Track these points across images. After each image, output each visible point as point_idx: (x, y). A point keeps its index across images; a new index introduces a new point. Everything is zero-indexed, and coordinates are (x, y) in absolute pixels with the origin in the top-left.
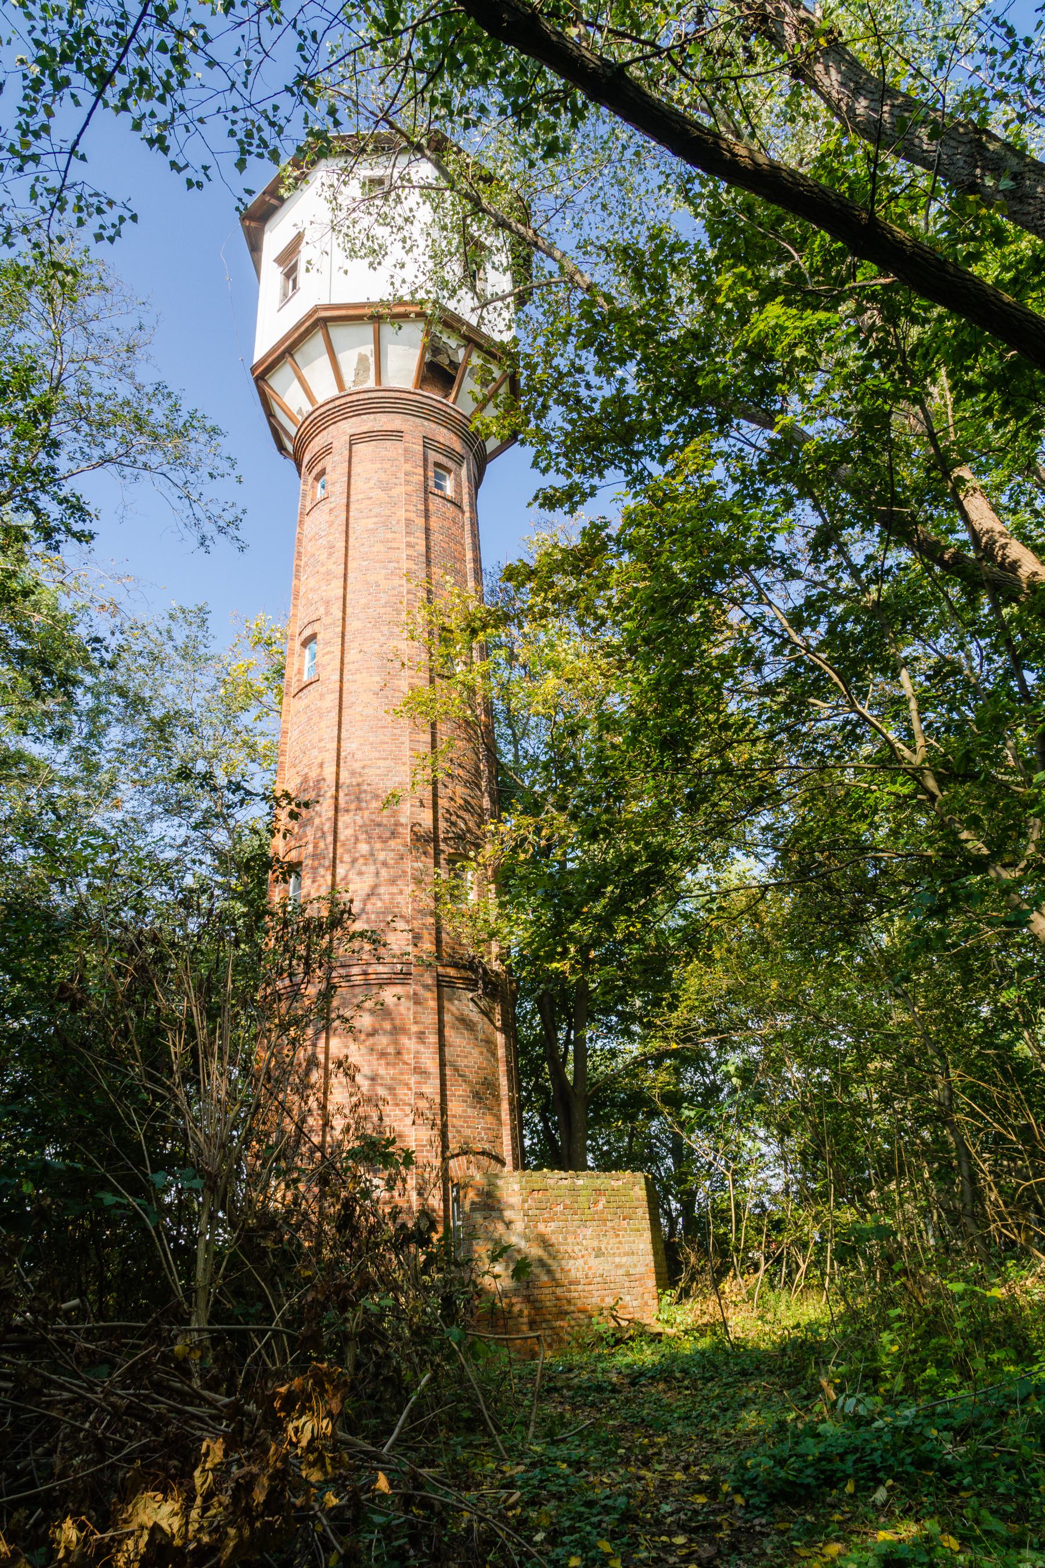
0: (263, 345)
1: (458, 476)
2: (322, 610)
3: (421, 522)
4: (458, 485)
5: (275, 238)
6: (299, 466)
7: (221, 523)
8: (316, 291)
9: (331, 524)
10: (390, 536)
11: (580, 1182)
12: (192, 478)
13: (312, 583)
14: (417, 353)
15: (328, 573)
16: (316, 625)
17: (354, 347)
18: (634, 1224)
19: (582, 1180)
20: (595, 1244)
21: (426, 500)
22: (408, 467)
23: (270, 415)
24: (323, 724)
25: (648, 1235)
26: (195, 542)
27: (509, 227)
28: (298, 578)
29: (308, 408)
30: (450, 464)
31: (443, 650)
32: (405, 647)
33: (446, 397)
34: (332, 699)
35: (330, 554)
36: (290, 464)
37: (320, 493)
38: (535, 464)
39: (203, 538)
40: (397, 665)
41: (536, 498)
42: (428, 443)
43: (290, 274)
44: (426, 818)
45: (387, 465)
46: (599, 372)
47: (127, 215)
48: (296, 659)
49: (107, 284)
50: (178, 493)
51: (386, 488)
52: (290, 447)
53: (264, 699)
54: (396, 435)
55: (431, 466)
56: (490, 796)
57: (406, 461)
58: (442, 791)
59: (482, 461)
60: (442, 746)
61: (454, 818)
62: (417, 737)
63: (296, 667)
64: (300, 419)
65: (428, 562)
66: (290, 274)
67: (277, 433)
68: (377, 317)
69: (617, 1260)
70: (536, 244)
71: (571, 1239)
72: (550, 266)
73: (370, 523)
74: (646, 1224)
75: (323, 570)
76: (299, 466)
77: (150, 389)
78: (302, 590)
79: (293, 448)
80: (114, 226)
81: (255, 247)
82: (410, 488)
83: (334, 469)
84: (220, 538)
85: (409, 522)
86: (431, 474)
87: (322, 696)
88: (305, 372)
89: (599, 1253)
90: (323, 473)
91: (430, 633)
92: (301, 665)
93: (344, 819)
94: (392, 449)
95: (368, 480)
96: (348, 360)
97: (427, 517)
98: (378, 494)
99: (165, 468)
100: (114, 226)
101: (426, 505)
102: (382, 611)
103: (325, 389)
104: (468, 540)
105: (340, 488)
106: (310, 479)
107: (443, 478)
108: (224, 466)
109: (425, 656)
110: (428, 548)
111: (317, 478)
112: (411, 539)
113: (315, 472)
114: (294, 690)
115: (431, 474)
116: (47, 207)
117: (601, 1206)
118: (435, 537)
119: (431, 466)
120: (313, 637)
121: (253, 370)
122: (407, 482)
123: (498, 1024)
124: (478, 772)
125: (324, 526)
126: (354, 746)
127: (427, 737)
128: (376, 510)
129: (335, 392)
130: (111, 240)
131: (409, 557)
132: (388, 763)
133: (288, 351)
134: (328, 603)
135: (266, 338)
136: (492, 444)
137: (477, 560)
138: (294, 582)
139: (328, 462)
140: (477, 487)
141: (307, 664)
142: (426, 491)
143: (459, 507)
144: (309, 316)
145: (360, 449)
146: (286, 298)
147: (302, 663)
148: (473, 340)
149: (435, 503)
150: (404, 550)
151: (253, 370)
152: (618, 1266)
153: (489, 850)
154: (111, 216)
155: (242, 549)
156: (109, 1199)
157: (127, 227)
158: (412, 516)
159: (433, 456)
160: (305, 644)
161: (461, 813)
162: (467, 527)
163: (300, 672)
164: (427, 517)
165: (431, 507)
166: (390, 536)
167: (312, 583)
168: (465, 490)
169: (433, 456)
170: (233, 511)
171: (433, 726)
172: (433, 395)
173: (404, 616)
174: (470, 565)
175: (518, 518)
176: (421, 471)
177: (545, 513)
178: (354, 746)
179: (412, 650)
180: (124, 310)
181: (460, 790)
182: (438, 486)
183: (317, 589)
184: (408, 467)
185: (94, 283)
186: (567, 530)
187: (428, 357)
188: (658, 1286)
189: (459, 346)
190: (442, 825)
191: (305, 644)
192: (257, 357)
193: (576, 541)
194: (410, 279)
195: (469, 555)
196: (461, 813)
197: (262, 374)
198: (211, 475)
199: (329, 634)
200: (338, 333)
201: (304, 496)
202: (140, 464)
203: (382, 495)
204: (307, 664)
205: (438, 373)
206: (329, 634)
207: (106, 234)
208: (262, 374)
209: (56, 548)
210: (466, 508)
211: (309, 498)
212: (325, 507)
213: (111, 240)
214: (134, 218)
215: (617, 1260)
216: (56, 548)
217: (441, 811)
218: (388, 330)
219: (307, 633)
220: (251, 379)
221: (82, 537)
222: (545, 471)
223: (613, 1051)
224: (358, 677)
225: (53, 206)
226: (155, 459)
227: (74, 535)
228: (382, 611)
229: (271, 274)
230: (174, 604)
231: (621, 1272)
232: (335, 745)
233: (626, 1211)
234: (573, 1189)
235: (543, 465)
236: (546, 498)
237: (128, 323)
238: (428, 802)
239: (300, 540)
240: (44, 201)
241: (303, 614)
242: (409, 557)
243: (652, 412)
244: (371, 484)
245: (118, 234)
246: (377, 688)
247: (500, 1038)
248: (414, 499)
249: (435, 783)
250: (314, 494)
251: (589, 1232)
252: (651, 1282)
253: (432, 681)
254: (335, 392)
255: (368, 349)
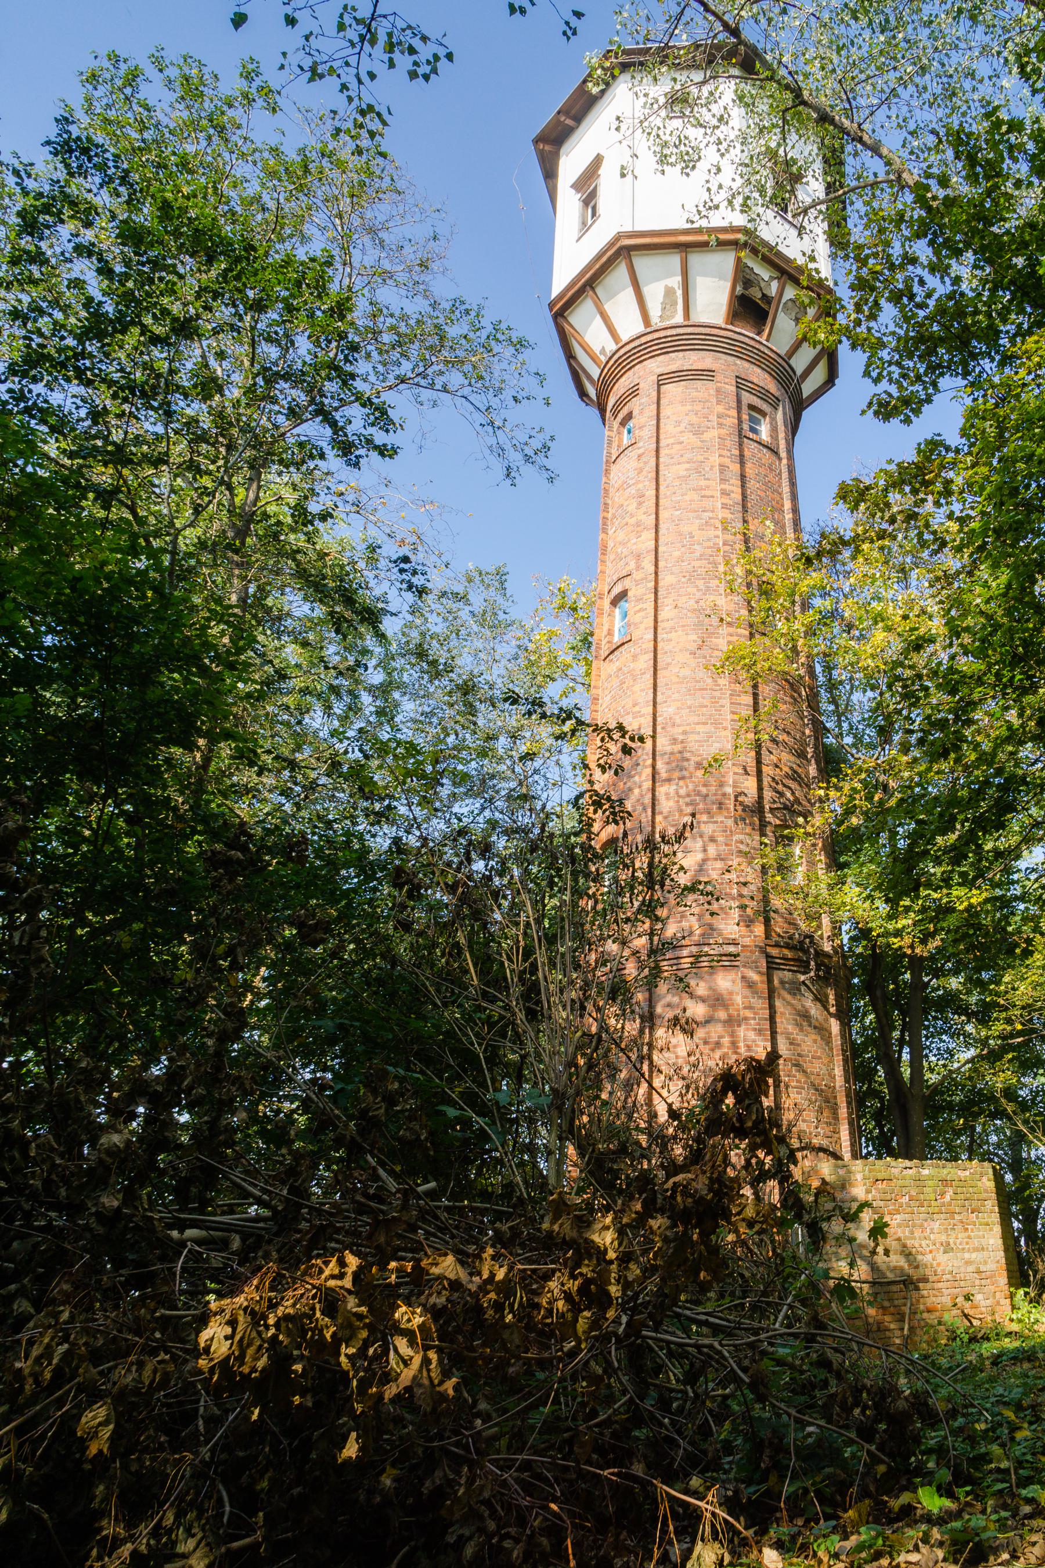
0: (561, 279)
1: (773, 420)
2: (632, 565)
3: (736, 468)
4: (774, 429)
5: (571, 163)
6: (602, 411)
7: (529, 451)
8: (622, 212)
9: (640, 471)
10: (703, 483)
11: (926, 1172)
12: (495, 402)
13: (621, 536)
14: (728, 285)
15: (638, 524)
16: (627, 581)
17: (660, 278)
18: (984, 1217)
19: (929, 1170)
20: (944, 1238)
21: (741, 445)
22: (720, 409)
23: (570, 356)
24: (637, 688)
25: (997, 1229)
26: (502, 472)
27: (832, 121)
28: (605, 531)
29: (611, 346)
30: (765, 407)
31: (764, 604)
32: (723, 602)
33: (759, 334)
34: (645, 661)
35: (640, 504)
36: (595, 412)
37: (626, 440)
38: (867, 374)
39: (508, 468)
40: (715, 620)
41: (870, 404)
42: (741, 383)
43: (590, 200)
44: (750, 785)
45: (698, 407)
46: (933, 269)
47: (442, 52)
48: (605, 619)
49: (401, 185)
50: (480, 418)
51: (698, 432)
52: (592, 392)
53: (570, 672)
54: (707, 374)
55: (745, 408)
56: (818, 763)
57: (719, 402)
58: (766, 758)
59: (799, 405)
60: (765, 706)
61: (780, 787)
62: (738, 700)
63: (605, 628)
64: (603, 359)
65: (745, 509)
66: (590, 200)
67: (577, 375)
68: (683, 246)
69: (967, 1255)
70: (860, 140)
71: (917, 1233)
72: (875, 166)
73: (681, 470)
74: (995, 1218)
75: (633, 521)
76: (602, 411)
77: (447, 306)
78: (610, 544)
79: (597, 394)
80: (428, 62)
81: (550, 174)
82: (723, 431)
83: (641, 412)
84: (527, 470)
85: (723, 468)
86: (745, 417)
87: (635, 657)
88: (607, 307)
89: (947, 1248)
90: (629, 416)
91: (749, 585)
92: (611, 625)
93: (662, 790)
94: (702, 389)
95: (678, 423)
96: (654, 293)
97: (742, 463)
98: (689, 438)
99: (466, 391)
100: (428, 62)
101: (741, 450)
102: (697, 564)
103: (630, 326)
104: (786, 489)
105: (649, 432)
106: (616, 424)
107: (758, 423)
108: (530, 384)
109: (744, 612)
110: (744, 496)
111: (623, 424)
112: (726, 487)
113: (621, 416)
114: (604, 653)
115: (745, 417)
116: (356, 40)
117: (948, 1198)
118: (752, 485)
119: (745, 408)
120: (623, 595)
121: (551, 306)
122: (720, 425)
123: (833, 1010)
124: (804, 744)
125: (631, 474)
126: (671, 710)
127: (749, 700)
128: (688, 456)
129: (640, 328)
130: (426, 77)
131: (724, 506)
132: (709, 728)
133: (588, 284)
134: (638, 557)
135: (564, 274)
136: (808, 388)
137: (795, 510)
138: (602, 536)
139: (635, 405)
140: (794, 434)
141: (618, 624)
142: (741, 435)
143: (776, 453)
144: (611, 244)
145: (671, 390)
146: (585, 227)
147: (612, 623)
148: (787, 271)
149: (750, 448)
150: (719, 498)
151: (551, 306)
152: (968, 1263)
153: (818, 820)
154: (425, 52)
155: (551, 480)
156: (452, 1112)
157: (443, 65)
158: (727, 461)
159: (747, 398)
160: (614, 603)
161: (786, 781)
162: (785, 475)
163: (610, 633)
164: (742, 463)
165: (746, 453)
166: (703, 483)
167: (621, 536)
168: (782, 435)
169: (747, 398)
170: (541, 436)
171: (755, 686)
172: (746, 332)
173: (722, 568)
174: (788, 516)
175: (849, 439)
176: (734, 413)
177: (877, 424)
178: (671, 710)
179: (729, 604)
180: (417, 218)
181: (785, 756)
182: (753, 430)
183: (627, 541)
184: (720, 409)
185: (386, 183)
186: (901, 443)
187: (739, 289)
188: (1010, 1284)
189: (772, 278)
190: (768, 794)
191: (614, 603)
192: (555, 292)
193: (910, 456)
194: (727, 182)
195: (787, 505)
196: (786, 781)
197: (561, 311)
198: (515, 399)
199: (640, 590)
200: (643, 264)
201: (610, 442)
202: (438, 387)
203: (693, 439)
204: (618, 624)
205: (750, 308)
206: (640, 590)
207: (420, 71)
208: (561, 311)
209: (357, 465)
210: (783, 454)
211: (615, 445)
212: (632, 453)
213: (426, 77)
214: (450, 57)
215: (967, 1255)
216: (357, 465)
217: (766, 781)
218: (696, 260)
219: (617, 590)
220: (549, 316)
221: (384, 451)
222: (876, 381)
223: (950, 1056)
224: (673, 635)
225: (362, 38)
226: (455, 378)
227: (376, 448)
228: (697, 564)
229: (568, 201)
230: (471, 566)
231: (971, 1269)
232: (650, 709)
233: (975, 1204)
234: (918, 1179)
235: (874, 374)
236: (880, 404)
237: (420, 232)
238: (752, 770)
239: (606, 491)
240: (352, 34)
241: (612, 571)
242: (724, 506)
243: (989, 315)
244: (682, 428)
245: (435, 71)
246: (693, 647)
247: (835, 1026)
248: (728, 443)
249: (758, 746)
250: (621, 440)
251: (936, 1226)
252: (1003, 1280)
253: (752, 636)
254: (640, 328)
255: (676, 282)
